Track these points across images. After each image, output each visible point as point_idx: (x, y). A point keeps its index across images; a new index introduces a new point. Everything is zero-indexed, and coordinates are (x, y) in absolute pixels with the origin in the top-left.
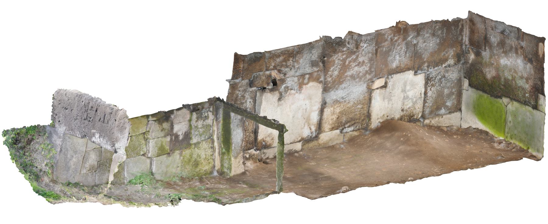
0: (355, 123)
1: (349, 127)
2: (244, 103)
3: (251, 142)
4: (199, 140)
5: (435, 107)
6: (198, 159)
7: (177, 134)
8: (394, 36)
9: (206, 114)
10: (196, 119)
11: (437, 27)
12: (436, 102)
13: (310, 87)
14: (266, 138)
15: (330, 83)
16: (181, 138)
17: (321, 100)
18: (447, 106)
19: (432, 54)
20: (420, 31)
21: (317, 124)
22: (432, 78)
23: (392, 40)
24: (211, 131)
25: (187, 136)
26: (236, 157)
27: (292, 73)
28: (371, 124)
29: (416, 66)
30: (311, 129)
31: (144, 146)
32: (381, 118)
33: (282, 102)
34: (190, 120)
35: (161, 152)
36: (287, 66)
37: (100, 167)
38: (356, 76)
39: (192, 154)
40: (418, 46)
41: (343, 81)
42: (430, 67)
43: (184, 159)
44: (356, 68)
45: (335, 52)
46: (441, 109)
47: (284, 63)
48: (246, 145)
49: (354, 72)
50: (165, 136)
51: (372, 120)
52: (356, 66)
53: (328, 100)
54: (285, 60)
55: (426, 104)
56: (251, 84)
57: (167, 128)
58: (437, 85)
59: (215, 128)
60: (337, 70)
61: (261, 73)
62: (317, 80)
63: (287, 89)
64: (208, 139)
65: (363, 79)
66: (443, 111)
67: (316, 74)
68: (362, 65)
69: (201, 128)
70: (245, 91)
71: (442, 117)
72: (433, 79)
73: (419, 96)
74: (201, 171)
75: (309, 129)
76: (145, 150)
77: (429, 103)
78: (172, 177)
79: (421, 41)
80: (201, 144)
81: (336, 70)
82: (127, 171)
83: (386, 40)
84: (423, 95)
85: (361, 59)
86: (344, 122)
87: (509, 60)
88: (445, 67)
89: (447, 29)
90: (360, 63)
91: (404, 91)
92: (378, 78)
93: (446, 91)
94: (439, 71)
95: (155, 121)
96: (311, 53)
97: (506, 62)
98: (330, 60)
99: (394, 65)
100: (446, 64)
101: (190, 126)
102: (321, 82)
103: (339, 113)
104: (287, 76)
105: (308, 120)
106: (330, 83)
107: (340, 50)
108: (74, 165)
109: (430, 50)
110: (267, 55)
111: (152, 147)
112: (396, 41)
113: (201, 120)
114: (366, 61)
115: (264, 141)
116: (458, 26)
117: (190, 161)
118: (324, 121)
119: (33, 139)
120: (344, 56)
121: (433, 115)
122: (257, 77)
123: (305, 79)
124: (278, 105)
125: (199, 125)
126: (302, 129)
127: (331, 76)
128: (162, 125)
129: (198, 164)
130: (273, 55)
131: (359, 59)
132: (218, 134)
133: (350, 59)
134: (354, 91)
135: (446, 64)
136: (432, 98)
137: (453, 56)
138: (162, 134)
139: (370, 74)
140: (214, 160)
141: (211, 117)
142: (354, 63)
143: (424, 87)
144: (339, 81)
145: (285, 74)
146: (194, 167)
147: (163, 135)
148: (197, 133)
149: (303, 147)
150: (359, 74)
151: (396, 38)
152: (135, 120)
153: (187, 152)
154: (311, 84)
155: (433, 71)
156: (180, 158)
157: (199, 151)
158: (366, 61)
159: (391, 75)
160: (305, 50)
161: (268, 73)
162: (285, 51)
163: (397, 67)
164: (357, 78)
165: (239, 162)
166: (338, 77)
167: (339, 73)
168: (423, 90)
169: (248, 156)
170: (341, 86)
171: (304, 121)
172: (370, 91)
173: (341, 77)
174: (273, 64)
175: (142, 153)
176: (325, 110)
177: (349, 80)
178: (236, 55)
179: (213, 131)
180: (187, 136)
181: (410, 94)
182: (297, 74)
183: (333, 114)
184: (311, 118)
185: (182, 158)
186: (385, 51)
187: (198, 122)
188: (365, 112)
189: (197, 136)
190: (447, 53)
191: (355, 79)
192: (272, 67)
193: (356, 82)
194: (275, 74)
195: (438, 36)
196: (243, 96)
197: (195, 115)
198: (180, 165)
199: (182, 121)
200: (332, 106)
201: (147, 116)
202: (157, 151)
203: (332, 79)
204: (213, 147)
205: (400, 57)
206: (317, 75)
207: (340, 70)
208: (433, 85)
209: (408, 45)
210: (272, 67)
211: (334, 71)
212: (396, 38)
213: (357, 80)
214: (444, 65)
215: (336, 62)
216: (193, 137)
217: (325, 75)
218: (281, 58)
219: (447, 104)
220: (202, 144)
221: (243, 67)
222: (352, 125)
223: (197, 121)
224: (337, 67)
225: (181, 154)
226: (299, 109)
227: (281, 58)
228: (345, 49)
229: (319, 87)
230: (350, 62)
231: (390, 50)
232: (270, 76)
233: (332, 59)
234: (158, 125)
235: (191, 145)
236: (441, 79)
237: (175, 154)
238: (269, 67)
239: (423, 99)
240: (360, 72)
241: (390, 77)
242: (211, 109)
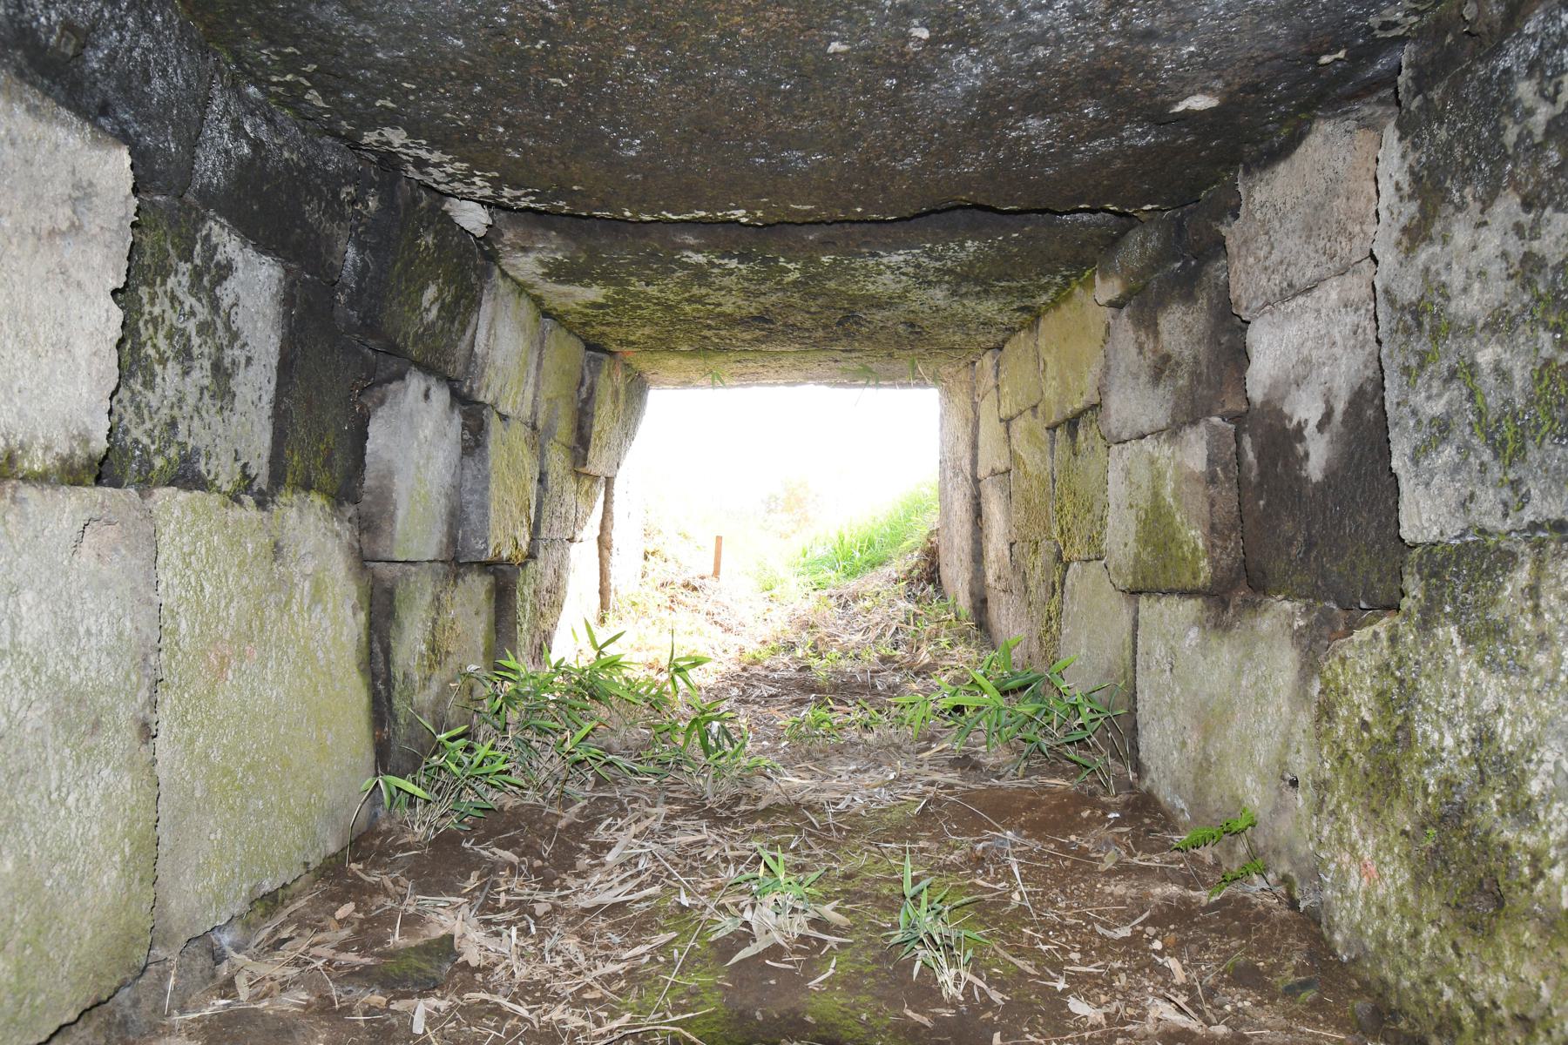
4: (1488, 509)
7: (1281, 416)
10: (1412, 208)
50: (1173, 431)
69: (1500, 324)
80: (1523, 576)
113: (1487, 203)
125: (1456, 279)
148: (1437, 408)
187: (1445, 240)
189: (1448, 453)
199: (1311, 273)
220: (1533, 591)
223: (1415, 235)
237: (1265, 623)
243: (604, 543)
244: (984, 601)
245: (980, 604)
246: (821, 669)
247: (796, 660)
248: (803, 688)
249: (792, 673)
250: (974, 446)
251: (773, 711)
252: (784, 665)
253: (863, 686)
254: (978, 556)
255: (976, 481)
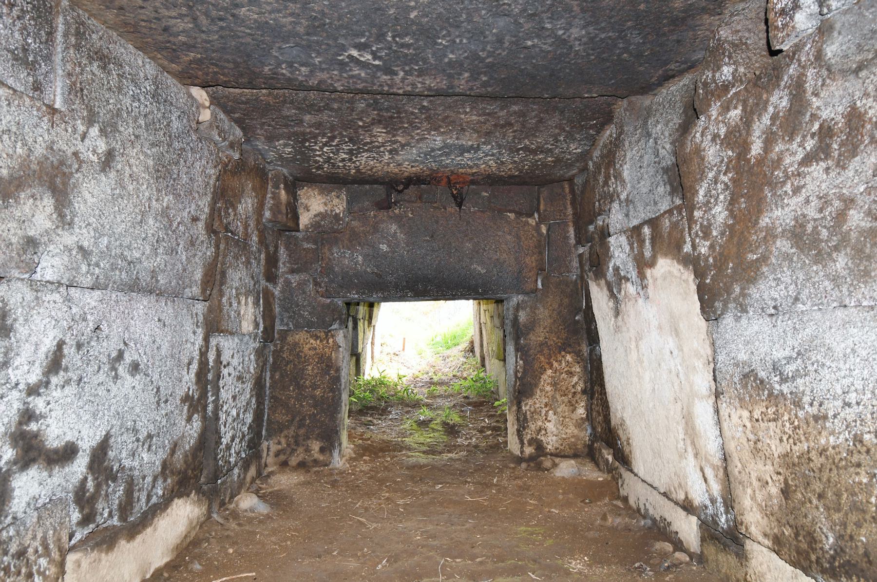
38: (824, 233)
49: (807, 201)
52: (808, 160)
60: (722, 197)
68: (852, 149)
90: (826, 132)
131: (816, 102)
133: (766, 120)
142: (791, 139)
150: (841, 217)
160: (627, 143)
164: (836, 248)
166: (731, 236)
177: (788, 257)
191: (821, 258)
207: (732, 194)
213: (841, 262)
224: (716, 181)
229: (686, 281)
233: (680, 66)
240: (849, 202)
243: (372, 344)
244: (484, 358)
245: (483, 359)
246: (436, 379)
247: (429, 376)
248: (431, 383)
249: (428, 380)
250: (480, 314)
251: (423, 389)
252: (426, 378)
253: (447, 383)
254: (482, 346)
255: (481, 324)
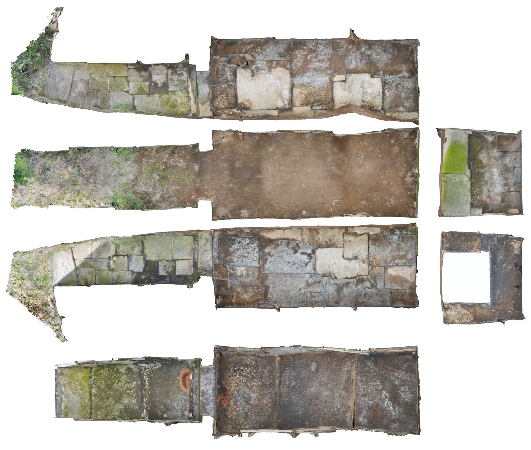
0: (322, 104)
1: (317, 106)
2: (224, 74)
3: (233, 104)
4: (175, 89)
5: (394, 105)
6: (175, 103)
8: (349, 45)
9: (181, 72)
11: (388, 46)
12: (394, 100)
13: (279, 71)
14: (244, 102)
15: (295, 70)
16: (160, 85)
17: (290, 82)
18: (405, 106)
19: (386, 65)
20: (371, 45)
21: (290, 99)
22: (389, 83)
23: (347, 47)
24: (186, 85)
25: (165, 85)
26: (203, 104)
27: (261, 57)
28: (335, 106)
29: (373, 71)
30: (284, 102)
31: (127, 86)
32: (344, 103)
33: (255, 77)
34: (167, 74)
35: (141, 92)
36: (257, 53)
37: (88, 94)
39: (170, 98)
40: (373, 57)
41: (307, 71)
42: (386, 75)
43: (162, 100)
44: (318, 64)
45: (297, 48)
46: (399, 107)
47: (254, 50)
48: (229, 105)
51: (335, 103)
52: (317, 62)
53: (295, 83)
54: (254, 48)
55: (385, 101)
56: (229, 62)
57: (146, 76)
58: (394, 89)
59: (190, 84)
61: (236, 55)
62: (284, 66)
63: (258, 69)
64: (184, 90)
65: (324, 72)
66: (401, 109)
67: (282, 62)
70: (224, 66)
71: (402, 113)
72: (390, 84)
73: (378, 94)
74: (178, 112)
75: (282, 102)
76: (128, 88)
77: (388, 101)
78: (152, 111)
79: (374, 54)
81: (299, 62)
82: (112, 101)
83: (342, 47)
84: (381, 94)
85: (321, 58)
86: (312, 101)
87: (497, 177)
88: (400, 77)
89: (397, 49)
91: (362, 87)
92: (338, 74)
93: (403, 95)
94: (395, 79)
95: (134, 69)
96: (277, 46)
97: (495, 174)
98: (294, 53)
99: (352, 67)
100: (401, 75)
101: (167, 78)
102: (287, 69)
103: (307, 94)
104: (257, 59)
105: (280, 95)
106: (295, 70)
107: (300, 47)
108: (62, 88)
109: (384, 62)
110: (239, 42)
111: (132, 87)
112: (350, 49)
114: (326, 60)
115: (243, 104)
116: (408, 50)
117: (167, 103)
118: (294, 98)
119: (38, 70)
120: (305, 53)
121: (392, 110)
122: (233, 57)
123: (273, 64)
124: (252, 80)
126: (276, 101)
127: (296, 66)
128: (140, 72)
129: (175, 106)
130: (244, 42)
132: (192, 88)
133: (311, 56)
134: (318, 80)
135: (401, 75)
136: (391, 97)
137: (406, 70)
138: (141, 79)
139: (330, 70)
140: (190, 106)
141: (185, 74)
143: (381, 87)
144: (303, 71)
145: (255, 58)
146: (171, 108)
147: (142, 80)
149: (280, 115)
151: (350, 47)
152: (117, 65)
153: (165, 97)
154: (279, 69)
155: (389, 78)
156: (159, 100)
157: (175, 97)
158: (326, 60)
159: (349, 73)
161: (242, 55)
162: (254, 41)
163: (354, 69)
165: (206, 108)
167: (303, 64)
168: (381, 91)
169: (231, 113)
170: (305, 74)
171: (277, 95)
172: (332, 82)
173: (305, 67)
174: (245, 49)
175: (125, 90)
176: (294, 90)
178: (213, 39)
179: (188, 85)
180: (165, 85)
181: (369, 90)
182: (267, 59)
183: (301, 93)
184: (283, 94)
185: (161, 100)
186: (342, 55)
188: (330, 97)
190: (400, 67)
192: (244, 51)
193: (319, 74)
194: (248, 57)
195: (390, 53)
196: (224, 70)
197: (170, 71)
198: (159, 104)
200: (299, 88)
201: (127, 65)
202: (136, 90)
203: (297, 68)
204: (188, 97)
205: (356, 62)
206: (283, 63)
208: (390, 88)
209: (362, 54)
210: (244, 51)
211: (298, 62)
212: (350, 47)
213: (319, 72)
214: (398, 76)
215: (299, 56)
216: (170, 86)
217: (291, 64)
218: (251, 46)
219: (405, 104)
221: (220, 48)
222: (320, 105)
223: (171, 75)
225: (160, 97)
226: (271, 86)
227: (251, 46)
228: (305, 48)
230: (311, 58)
231: (346, 55)
232: (244, 58)
234: (136, 72)
235: (169, 92)
236: (397, 85)
238: (241, 51)
239: (381, 96)
240: (322, 67)
241: (348, 75)
242: (185, 69)
